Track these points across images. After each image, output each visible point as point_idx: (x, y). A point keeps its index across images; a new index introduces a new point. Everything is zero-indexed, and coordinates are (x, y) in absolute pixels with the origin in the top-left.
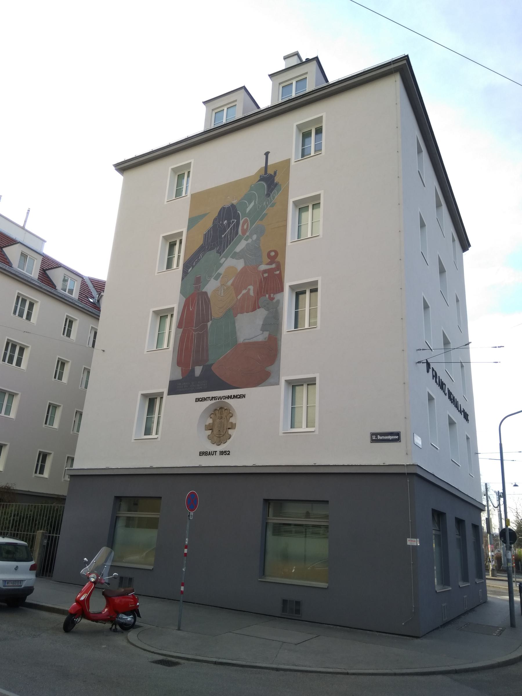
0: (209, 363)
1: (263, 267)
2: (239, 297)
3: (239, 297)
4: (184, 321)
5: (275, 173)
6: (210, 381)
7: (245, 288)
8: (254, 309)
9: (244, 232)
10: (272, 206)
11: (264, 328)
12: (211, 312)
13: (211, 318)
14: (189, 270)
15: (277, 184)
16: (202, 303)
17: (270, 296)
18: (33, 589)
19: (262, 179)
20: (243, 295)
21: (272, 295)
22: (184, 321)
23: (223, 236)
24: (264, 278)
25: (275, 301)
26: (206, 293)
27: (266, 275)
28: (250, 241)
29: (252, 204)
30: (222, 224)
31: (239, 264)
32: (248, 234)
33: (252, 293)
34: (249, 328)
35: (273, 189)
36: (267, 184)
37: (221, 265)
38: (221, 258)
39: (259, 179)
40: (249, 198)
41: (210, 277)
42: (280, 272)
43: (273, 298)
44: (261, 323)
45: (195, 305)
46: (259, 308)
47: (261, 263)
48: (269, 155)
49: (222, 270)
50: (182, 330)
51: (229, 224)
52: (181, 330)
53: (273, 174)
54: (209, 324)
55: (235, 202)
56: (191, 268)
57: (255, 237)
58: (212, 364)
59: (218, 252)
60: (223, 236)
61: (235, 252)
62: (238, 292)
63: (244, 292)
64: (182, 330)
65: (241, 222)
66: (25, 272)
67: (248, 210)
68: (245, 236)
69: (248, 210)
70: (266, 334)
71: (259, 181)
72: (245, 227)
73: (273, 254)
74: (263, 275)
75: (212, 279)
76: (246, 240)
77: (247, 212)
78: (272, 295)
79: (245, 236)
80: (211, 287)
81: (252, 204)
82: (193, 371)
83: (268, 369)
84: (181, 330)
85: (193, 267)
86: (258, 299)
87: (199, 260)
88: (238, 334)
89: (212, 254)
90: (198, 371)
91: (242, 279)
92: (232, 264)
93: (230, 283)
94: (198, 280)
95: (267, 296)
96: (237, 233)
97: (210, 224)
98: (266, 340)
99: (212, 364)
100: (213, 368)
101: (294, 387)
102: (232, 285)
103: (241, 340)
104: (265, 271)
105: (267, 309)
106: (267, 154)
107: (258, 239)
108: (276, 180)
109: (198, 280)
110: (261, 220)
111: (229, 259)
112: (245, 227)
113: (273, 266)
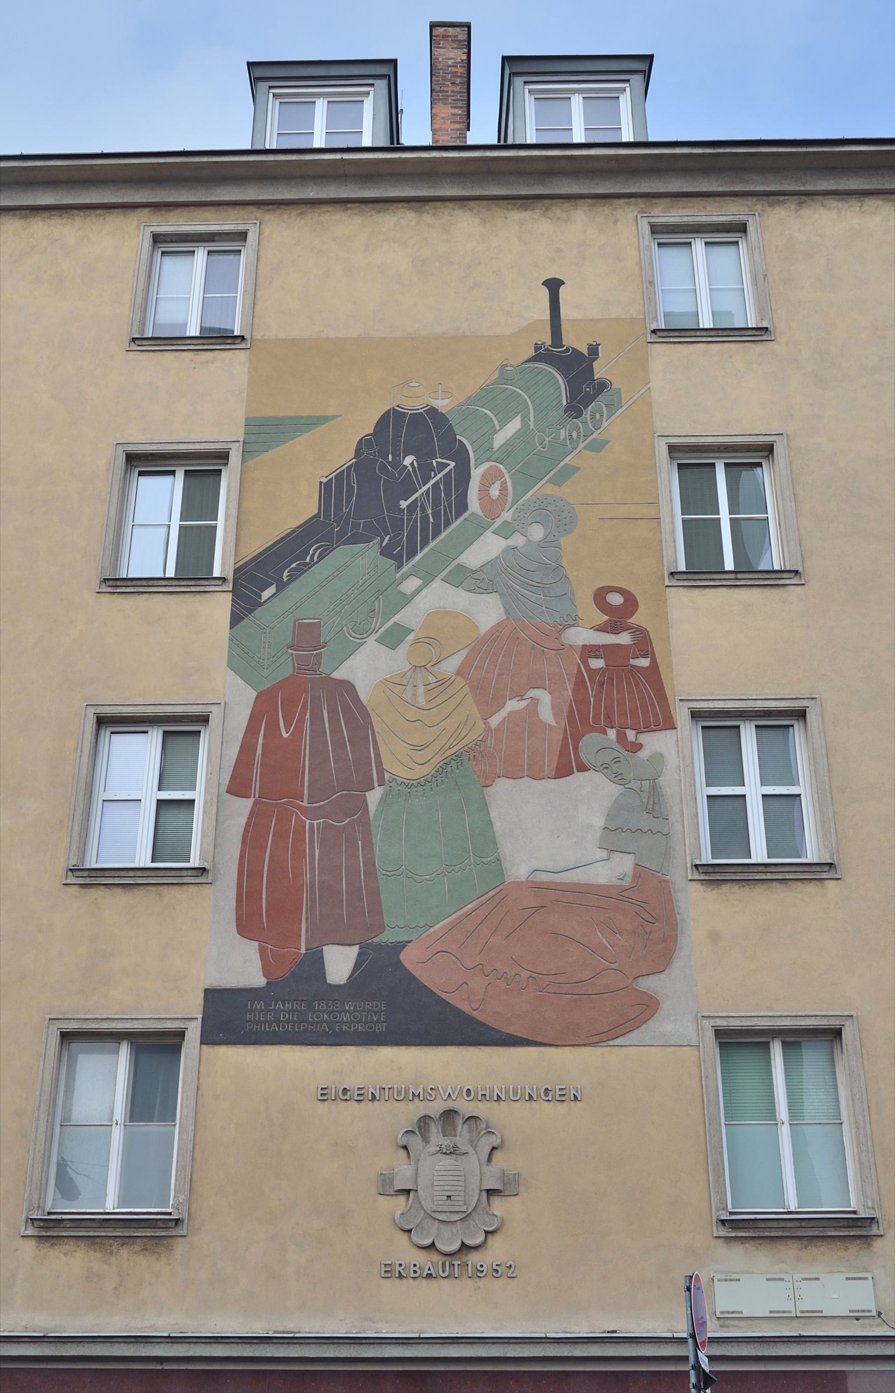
0: (388, 937)
1: (582, 636)
2: (495, 721)
3: (495, 721)
4: (256, 772)
5: (594, 350)
6: (398, 1008)
9: (492, 508)
10: (598, 446)
11: (614, 837)
14: (266, 595)
15: (602, 386)
16: (334, 720)
17: (621, 738)
20: (511, 714)
21: (631, 735)
22: (256, 772)
23: (404, 504)
24: (592, 672)
25: (643, 754)
26: (348, 687)
27: (597, 663)
28: (518, 540)
29: (514, 426)
30: (397, 463)
31: (488, 612)
32: (507, 515)
33: (546, 713)
34: (553, 831)
35: (587, 400)
37: (408, 599)
38: (405, 577)
39: (531, 353)
40: (496, 398)
41: (364, 633)
42: (654, 661)
43: (636, 747)
44: (598, 821)
45: (301, 720)
46: (583, 768)
47: (574, 621)
50: (248, 803)
51: (426, 471)
52: (242, 807)
53: (585, 351)
54: (374, 797)
55: (442, 404)
56: (272, 590)
57: (537, 532)
58: (403, 945)
59: (386, 552)
60: (404, 504)
61: (460, 566)
62: (489, 701)
63: (513, 705)
64: (248, 803)
65: (476, 474)
66: (239, 295)
67: (499, 440)
69: (499, 440)
70: (624, 865)
71: (532, 359)
72: (495, 492)
73: (616, 599)
74: (586, 664)
75: (371, 641)
76: (505, 531)
78: (631, 735)
79: (499, 522)
81: (514, 426)
83: (647, 984)
84: (242, 807)
86: (577, 739)
88: (506, 848)
89: (361, 559)
90: (339, 963)
91: (495, 664)
92: (449, 601)
94: (308, 638)
95: (612, 734)
96: (462, 506)
97: (343, 455)
98: (627, 882)
99: (403, 945)
100: (407, 958)
103: (519, 870)
104: (590, 651)
105: (618, 778)
106: (554, 286)
107: (550, 541)
108: (600, 370)
109: (308, 638)
110: (558, 481)
112: (495, 492)
113: (624, 638)
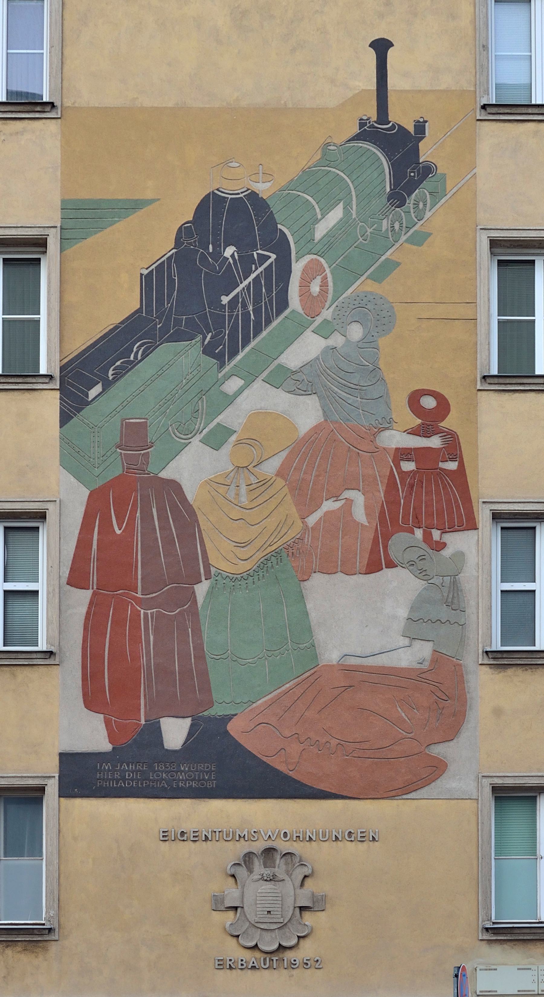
0: (217, 711)
1: (396, 439)
2: (312, 520)
3: (312, 520)
4: (93, 566)
5: (420, 127)
6: (225, 767)
7: (337, 498)
8: (373, 567)
9: (313, 305)
10: (419, 239)
12: (204, 552)
13: (207, 566)
14: (93, 393)
17: (427, 537)
18: (373, 42)
19: (367, 133)
21: (436, 534)
22: (93, 566)
23: (225, 300)
25: (446, 553)
26: (174, 487)
27: (408, 466)
28: (337, 340)
29: (336, 215)
30: (218, 255)
32: (327, 314)
33: (360, 514)
36: (389, 155)
37: (230, 400)
39: (355, 130)
42: (462, 465)
43: (440, 546)
44: (403, 613)
46: (391, 565)
47: (388, 424)
48: (391, 53)
49: (231, 417)
50: (85, 595)
51: (247, 262)
53: (411, 129)
54: (201, 589)
55: (263, 189)
57: (356, 332)
58: (229, 718)
59: (208, 351)
61: (280, 367)
63: (329, 505)
64: (85, 595)
65: (297, 268)
68: (319, 320)
69: (321, 230)
70: (423, 651)
72: (315, 288)
74: (398, 467)
75: (196, 441)
76: (325, 331)
77: (318, 235)
78: (436, 534)
80: (192, 468)
81: (336, 215)
82: (154, 730)
83: (438, 750)
85: (107, 385)
86: (387, 537)
87: (134, 364)
88: (320, 635)
89: (182, 358)
90: (175, 733)
91: (312, 466)
92: (268, 405)
93: (271, 467)
94: (135, 437)
95: (419, 533)
97: (163, 246)
99: (229, 718)
101: (300, 910)
102: (280, 473)
103: (331, 655)
104: (403, 454)
105: (422, 574)
106: (381, 47)
107: (368, 342)
108: (427, 152)
111: (258, 384)
112: (315, 288)
113: (435, 442)
